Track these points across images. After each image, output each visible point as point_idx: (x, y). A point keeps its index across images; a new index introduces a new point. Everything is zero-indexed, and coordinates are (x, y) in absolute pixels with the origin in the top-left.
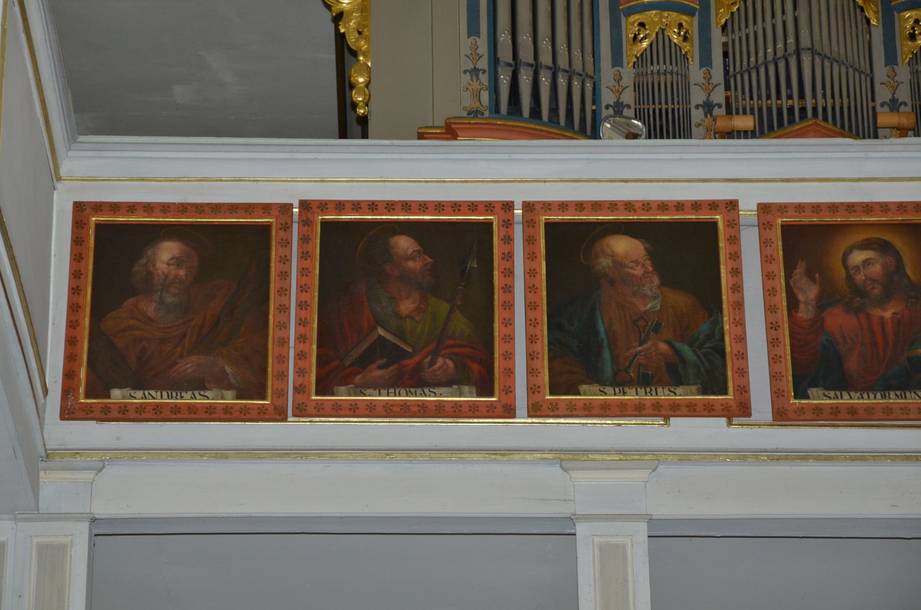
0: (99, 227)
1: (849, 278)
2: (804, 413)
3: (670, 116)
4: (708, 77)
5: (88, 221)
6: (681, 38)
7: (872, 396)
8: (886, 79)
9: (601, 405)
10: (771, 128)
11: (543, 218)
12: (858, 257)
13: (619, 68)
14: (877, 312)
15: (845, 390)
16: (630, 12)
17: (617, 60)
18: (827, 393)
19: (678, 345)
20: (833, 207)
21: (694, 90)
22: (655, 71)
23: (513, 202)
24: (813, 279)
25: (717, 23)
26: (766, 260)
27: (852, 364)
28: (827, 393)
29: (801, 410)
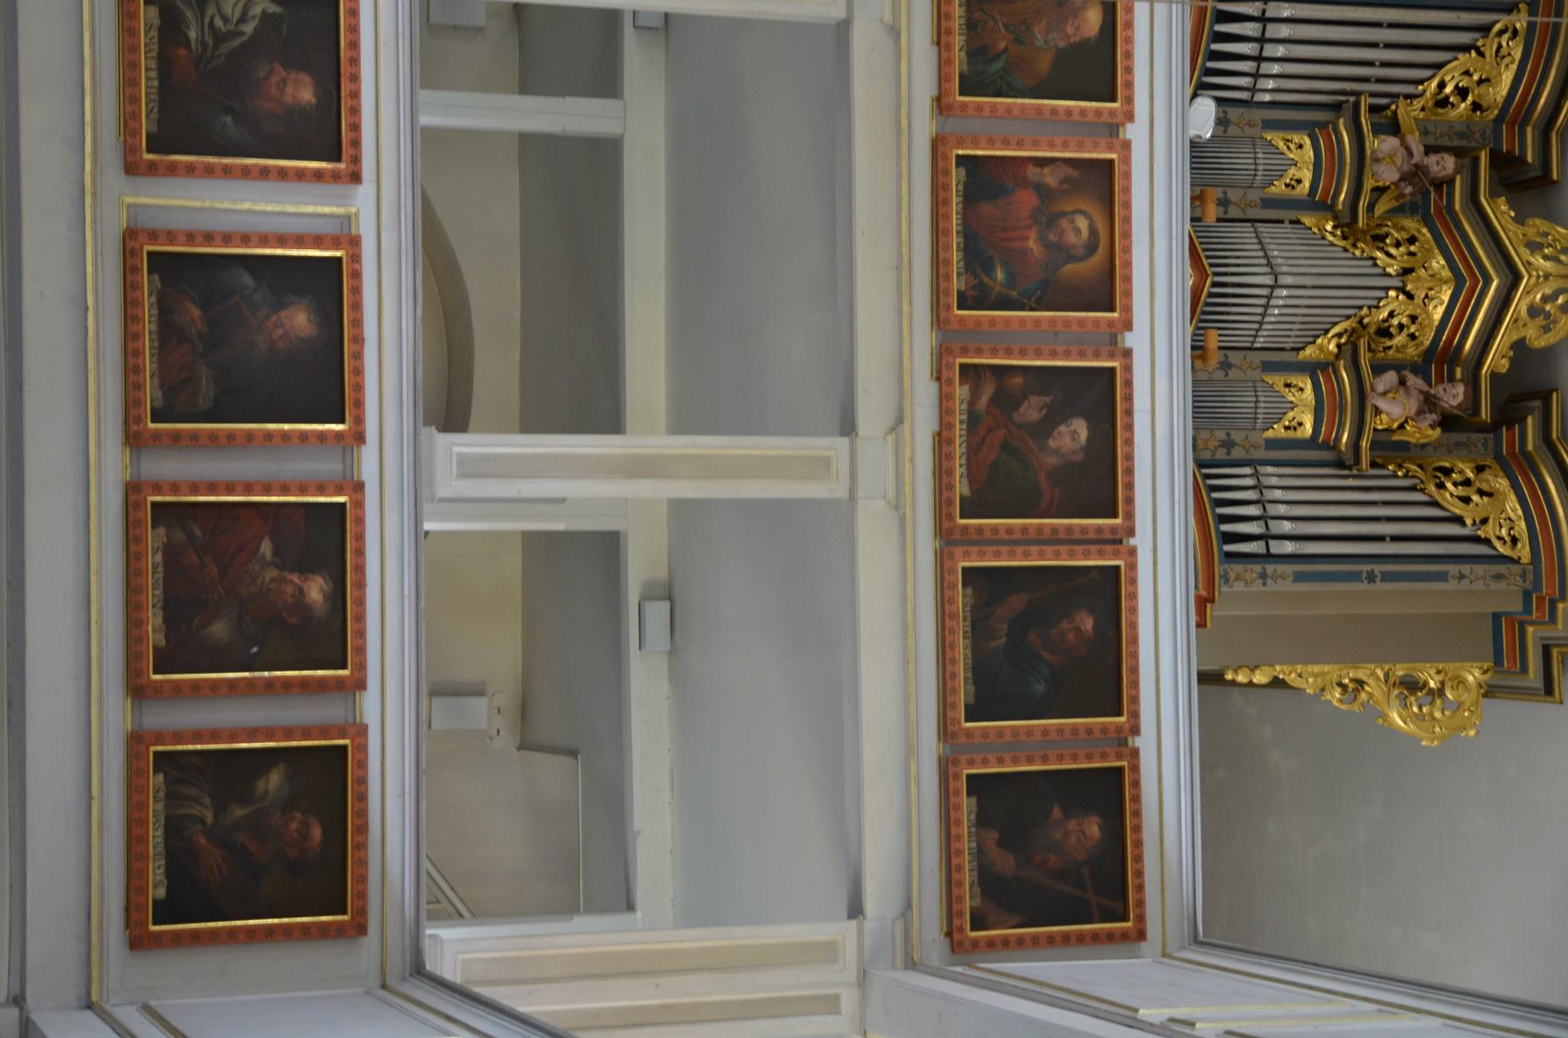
1: (1063, 214)
12: (1083, 224)
14: (1033, 235)
19: (1003, 58)
24: (1062, 183)
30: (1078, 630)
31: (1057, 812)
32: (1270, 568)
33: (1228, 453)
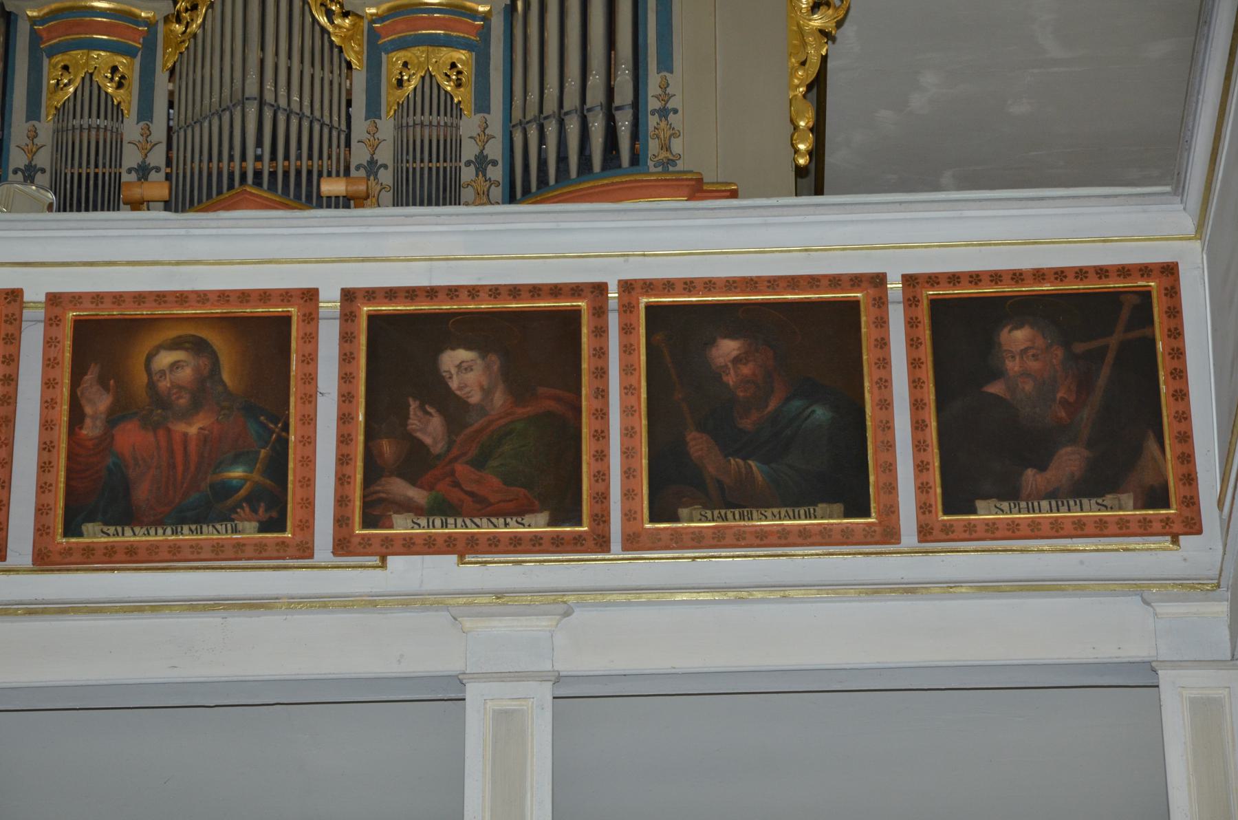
0: (372, 318)
1: (151, 385)
2: (71, 555)
3: (92, 183)
4: (147, 133)
5: (638, 303)
6: (114, 85)
7: (160, 531)
8: (365, 136)
9: (756, 532)
10: (526, 191)
11: (644, 300)
12: (165, 359)
13: (35, 123)
14: (180, 428)
15: (128, 524)
16: (52, 52)
17: (373, 111)
18: (105, 529)
20: (139, 298)
21: (127, 149)
22: (77, 126)
23: (316, 290)
24: (106, 388)
25: (164, 65)
26: (50, 363)
27: (142, 492)
28: (105, 529)
29: (69, 551)
30: (737, 360)
31: (996, 388)
32: (653, 104)
33: (494, 163)
